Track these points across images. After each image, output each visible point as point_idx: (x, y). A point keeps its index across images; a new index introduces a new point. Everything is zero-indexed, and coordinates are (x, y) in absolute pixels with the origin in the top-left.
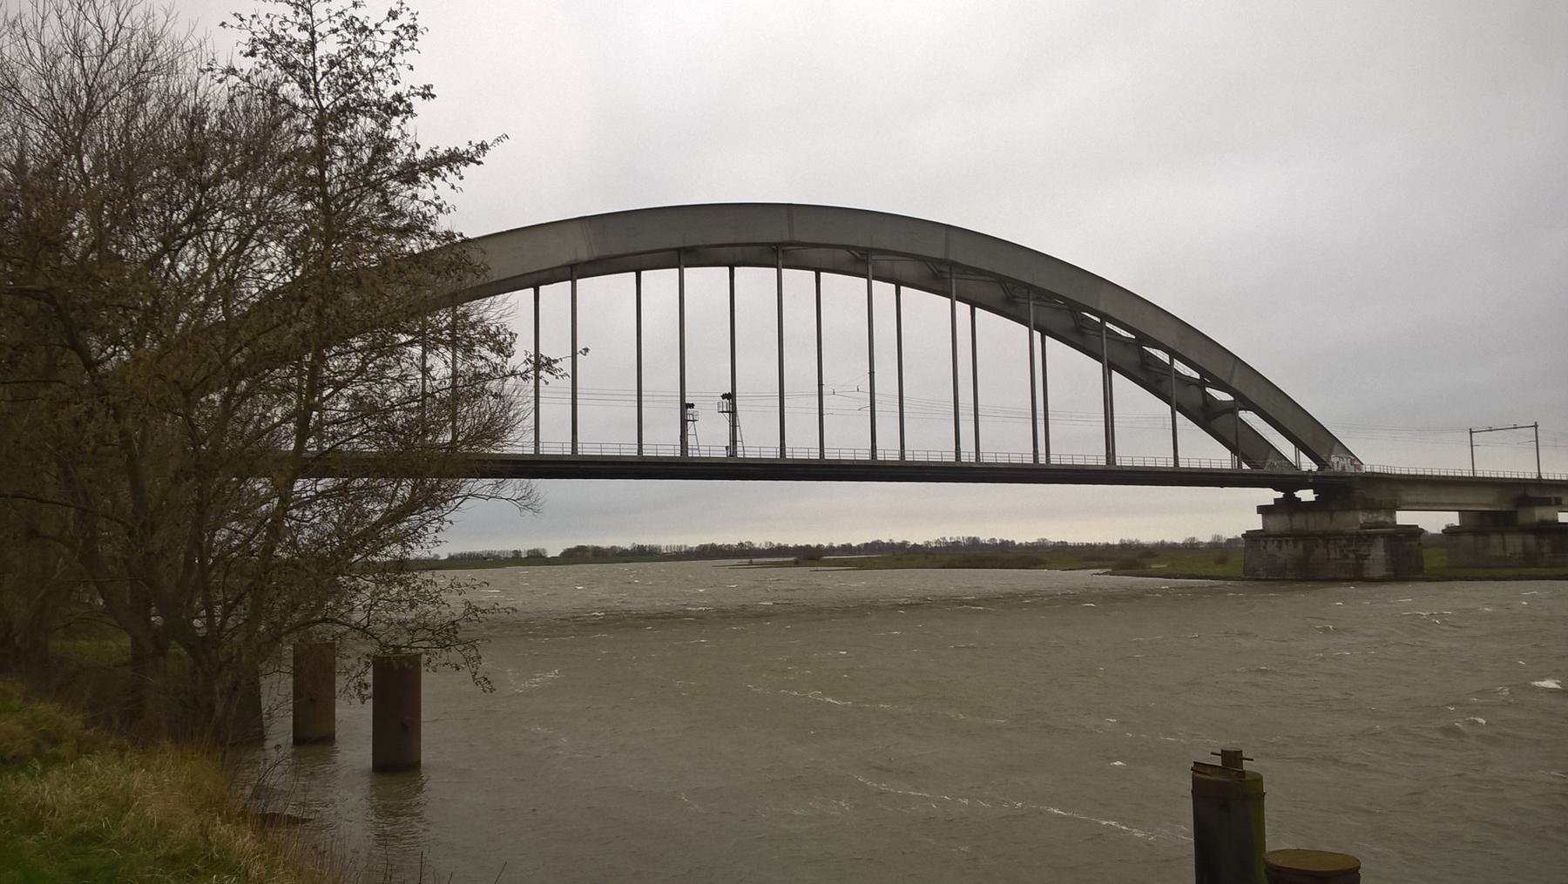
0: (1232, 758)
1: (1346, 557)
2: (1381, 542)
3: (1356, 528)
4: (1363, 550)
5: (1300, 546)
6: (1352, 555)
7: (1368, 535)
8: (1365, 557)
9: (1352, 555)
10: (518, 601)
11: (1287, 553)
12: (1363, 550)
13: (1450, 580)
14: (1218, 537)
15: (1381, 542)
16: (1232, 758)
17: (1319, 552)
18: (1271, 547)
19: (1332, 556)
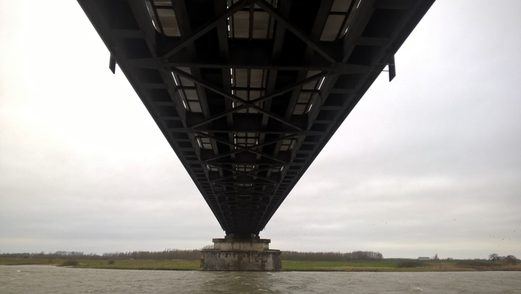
0: (213, 240)
1: (257, 261)
2: (271, 256)
3: (262, 250)
4: (265, 259)
5: (236, 256)
6: (260, 261)
7: (267, 253)
8: (266, 261)
9: (260, 261)
10: (189, 262)
11: (231, 259)
12: (265, 259)
13: (325, 22)
14: (83, 253)
15: (271, 256)
16: (213, 240)
17: (245, 259)
18: (222, 256)
19: (251, 261)
